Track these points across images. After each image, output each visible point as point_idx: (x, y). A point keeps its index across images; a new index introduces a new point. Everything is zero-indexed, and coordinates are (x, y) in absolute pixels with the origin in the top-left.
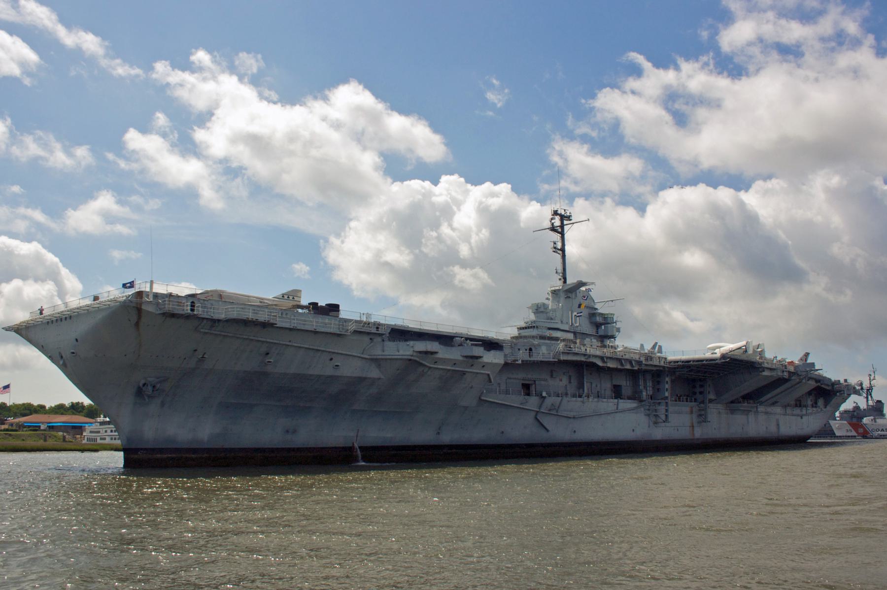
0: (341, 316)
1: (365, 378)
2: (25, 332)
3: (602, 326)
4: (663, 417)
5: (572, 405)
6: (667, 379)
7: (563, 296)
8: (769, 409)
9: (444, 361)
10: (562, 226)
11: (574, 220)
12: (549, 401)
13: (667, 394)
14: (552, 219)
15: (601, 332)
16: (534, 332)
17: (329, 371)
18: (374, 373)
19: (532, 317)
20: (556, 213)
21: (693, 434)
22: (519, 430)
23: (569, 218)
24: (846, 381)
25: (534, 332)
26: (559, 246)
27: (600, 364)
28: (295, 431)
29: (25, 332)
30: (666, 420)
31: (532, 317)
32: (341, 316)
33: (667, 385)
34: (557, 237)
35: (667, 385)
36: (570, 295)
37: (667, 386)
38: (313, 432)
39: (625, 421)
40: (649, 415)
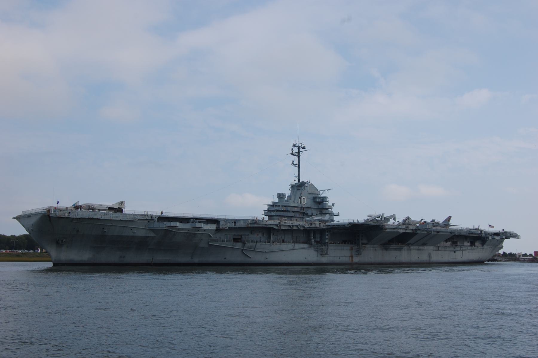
0: (52, 262)
1: (148, 237)
2: (18, 218)
3: (320, 204)
4: (326, 252)
5: (265, 246)
6: (327, 233)
7: (296, 188)
8: (421, 248)
9: (183, 229)
10: (299, 152)
11: (307, 148)
12: (248, 244)
13: (327, 241)
14: (292, 149)
15: (320, 206)
16: (275, 208)
17: (132, 234)
18: (152, 234)
19: (277, 200)
20: (295, 146)
21: (352, 260)
22: (237, 258)
23: (304, 148)
24: (503, 230)
25: (275, 208)
26: (296, 162)
27: (276, 228)
28: (124, 257)
29: (18, 218)
30: (327, 254)
31: (277, 200)
32: (52, 262)
33: (327, 236)
34: (296, 159)
35: (327, 236)
36: (300, 188)
37: (327, 237)
38: (131, 257)
39: (303, 253)
40: (317, 251)
